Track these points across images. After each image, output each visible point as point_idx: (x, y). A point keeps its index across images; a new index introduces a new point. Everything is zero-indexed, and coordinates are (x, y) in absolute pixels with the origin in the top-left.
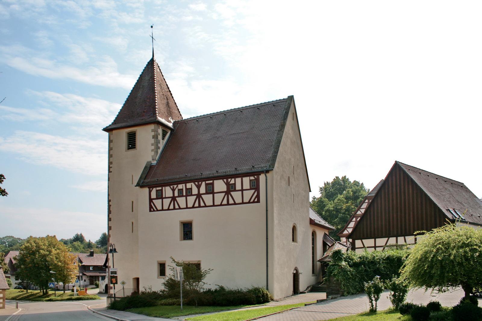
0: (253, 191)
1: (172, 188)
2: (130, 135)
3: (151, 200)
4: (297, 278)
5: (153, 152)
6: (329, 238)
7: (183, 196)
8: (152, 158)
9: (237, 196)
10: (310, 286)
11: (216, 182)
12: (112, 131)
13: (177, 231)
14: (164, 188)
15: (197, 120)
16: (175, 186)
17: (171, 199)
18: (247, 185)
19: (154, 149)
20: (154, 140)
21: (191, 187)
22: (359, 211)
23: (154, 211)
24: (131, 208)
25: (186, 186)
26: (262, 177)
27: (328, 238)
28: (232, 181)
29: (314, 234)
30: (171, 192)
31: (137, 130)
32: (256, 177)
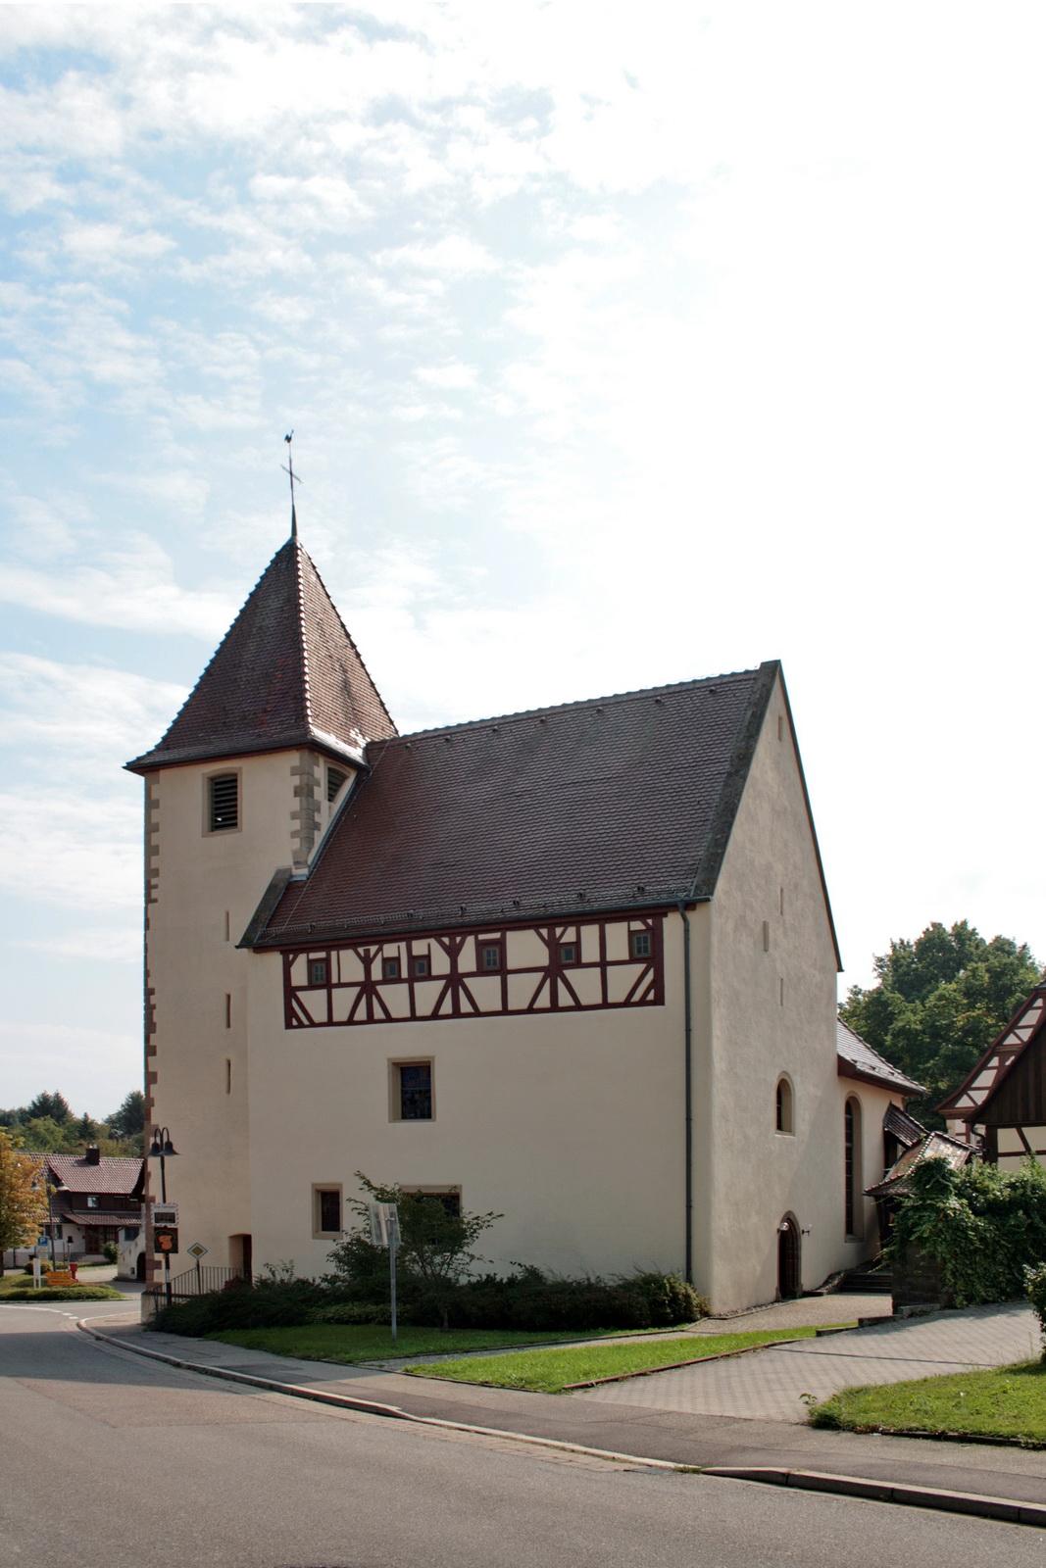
0: (640, 968)
1: (362, 954)
2: (217, 784)
3: (290, 992)
5: (297, 840)
7: (399, 980)
8: (294, 858)
9: (585, 983)
10: (839, 1273)
12: (158, 770)
13: (381, 1091)
14: (334, 954)
16: (373, 949)
17: (443, 982)
20: (301, 801)
21: (426, 953)
22: (965, 1097)
23: (301, 1025)
25: (409, 949)
27: (903, 1119)
28: (570, 935)
29: (852, 1108)
30: (360, 967)
31: (240, 768)
32: (650, 921)
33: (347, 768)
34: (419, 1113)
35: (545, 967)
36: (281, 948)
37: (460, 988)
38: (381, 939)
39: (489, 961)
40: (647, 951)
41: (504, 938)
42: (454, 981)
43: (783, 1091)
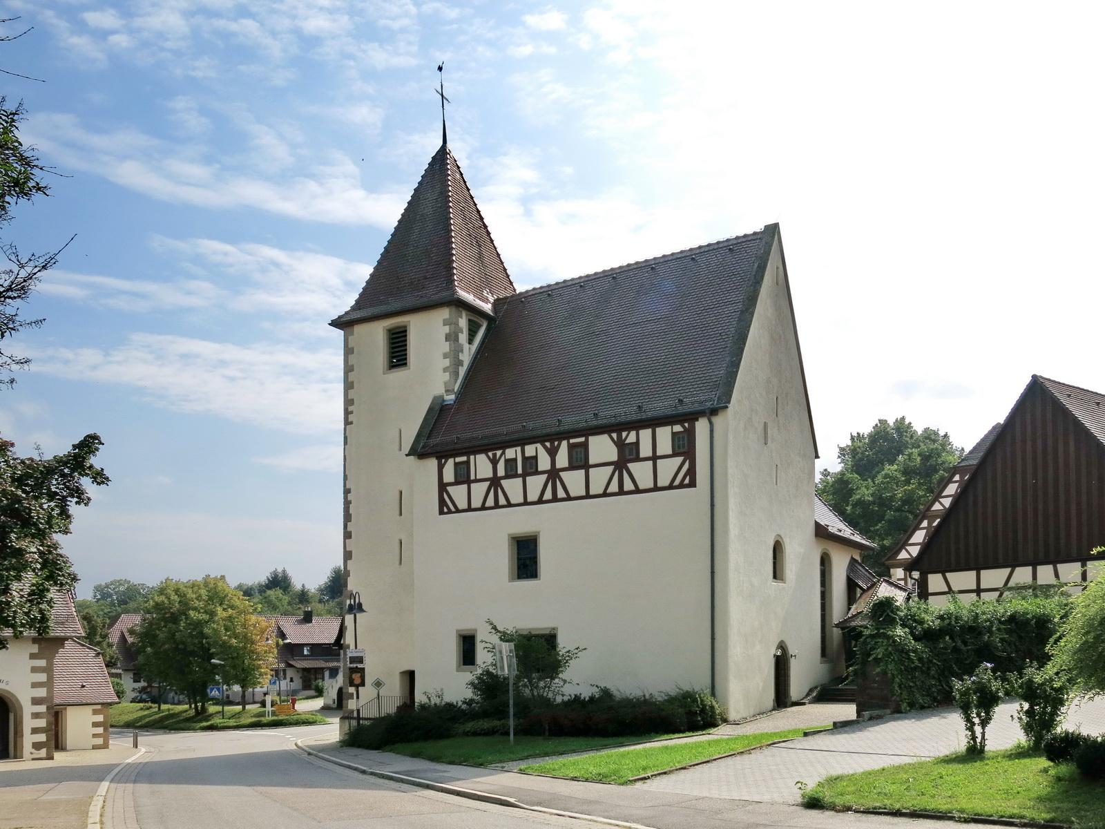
0: (679, 460)
3: (443, 487)
6: (863, 571)
7: (516, 476)
9: (641, 472)
10: (816, 687)
11: (593, 440)
12: (353, 325)
13: (503, 558)
14: (472, 457)
15: (550, 293)
16: (499, 453)
18: (665, 446)
20: (450, 345)
23: (450, 512)
28: (632, 438)
29: (825, 561)
30: (490, 466)
32: (686, 425)
36: (438, 455)
37: (445, 494)
38: (504, 445)
39: (683, 440)
40: (685, 447)
41: (587, 442)
42: (554, 474)
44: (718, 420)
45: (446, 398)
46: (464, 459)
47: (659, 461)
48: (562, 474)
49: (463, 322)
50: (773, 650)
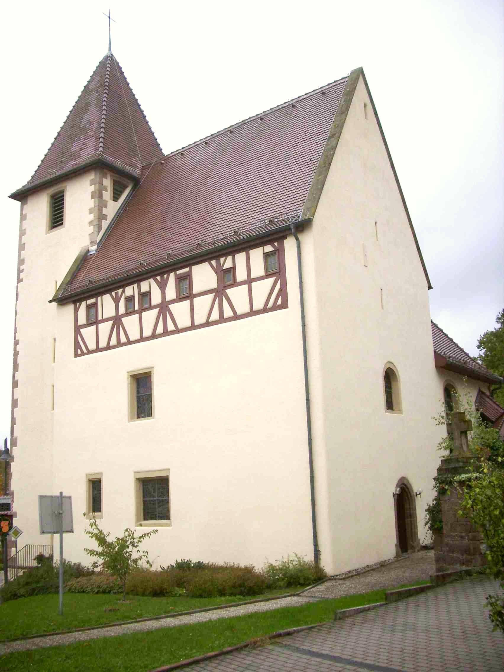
0: (272, 280)
2: (55, 199)
3: (77, 329)
4: (410, 508)
5: (92, 227)
7: (133, 312)
9: (238, 295)
11: (196, 269)
13: (123, 395)
15: (181, 153)
16: (120, 291)
18: (258, 269)
19: (95, 219)
20: (95, 201)
23: (83, 354)
24: (53, 349)
26: (289, 244)
28: (228, 263)
30: (113, 304)
32: (276, 244)
33: (127, 180)
34: (146, 414)
35: (215, 289)
40: (275, 269)
42: (164, 308)
43: (390, 377)
44: (308, 240)
45: (91, 248)
46: (93, 300)
47: (253, 284)
48: (171, 307)
49: (108, 182)
50: (392, 488)
